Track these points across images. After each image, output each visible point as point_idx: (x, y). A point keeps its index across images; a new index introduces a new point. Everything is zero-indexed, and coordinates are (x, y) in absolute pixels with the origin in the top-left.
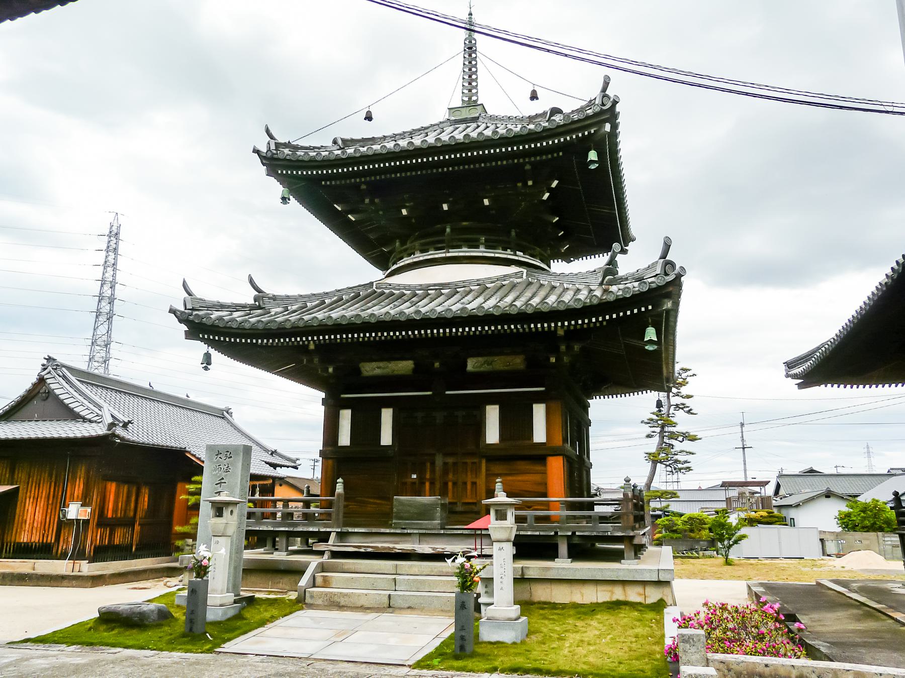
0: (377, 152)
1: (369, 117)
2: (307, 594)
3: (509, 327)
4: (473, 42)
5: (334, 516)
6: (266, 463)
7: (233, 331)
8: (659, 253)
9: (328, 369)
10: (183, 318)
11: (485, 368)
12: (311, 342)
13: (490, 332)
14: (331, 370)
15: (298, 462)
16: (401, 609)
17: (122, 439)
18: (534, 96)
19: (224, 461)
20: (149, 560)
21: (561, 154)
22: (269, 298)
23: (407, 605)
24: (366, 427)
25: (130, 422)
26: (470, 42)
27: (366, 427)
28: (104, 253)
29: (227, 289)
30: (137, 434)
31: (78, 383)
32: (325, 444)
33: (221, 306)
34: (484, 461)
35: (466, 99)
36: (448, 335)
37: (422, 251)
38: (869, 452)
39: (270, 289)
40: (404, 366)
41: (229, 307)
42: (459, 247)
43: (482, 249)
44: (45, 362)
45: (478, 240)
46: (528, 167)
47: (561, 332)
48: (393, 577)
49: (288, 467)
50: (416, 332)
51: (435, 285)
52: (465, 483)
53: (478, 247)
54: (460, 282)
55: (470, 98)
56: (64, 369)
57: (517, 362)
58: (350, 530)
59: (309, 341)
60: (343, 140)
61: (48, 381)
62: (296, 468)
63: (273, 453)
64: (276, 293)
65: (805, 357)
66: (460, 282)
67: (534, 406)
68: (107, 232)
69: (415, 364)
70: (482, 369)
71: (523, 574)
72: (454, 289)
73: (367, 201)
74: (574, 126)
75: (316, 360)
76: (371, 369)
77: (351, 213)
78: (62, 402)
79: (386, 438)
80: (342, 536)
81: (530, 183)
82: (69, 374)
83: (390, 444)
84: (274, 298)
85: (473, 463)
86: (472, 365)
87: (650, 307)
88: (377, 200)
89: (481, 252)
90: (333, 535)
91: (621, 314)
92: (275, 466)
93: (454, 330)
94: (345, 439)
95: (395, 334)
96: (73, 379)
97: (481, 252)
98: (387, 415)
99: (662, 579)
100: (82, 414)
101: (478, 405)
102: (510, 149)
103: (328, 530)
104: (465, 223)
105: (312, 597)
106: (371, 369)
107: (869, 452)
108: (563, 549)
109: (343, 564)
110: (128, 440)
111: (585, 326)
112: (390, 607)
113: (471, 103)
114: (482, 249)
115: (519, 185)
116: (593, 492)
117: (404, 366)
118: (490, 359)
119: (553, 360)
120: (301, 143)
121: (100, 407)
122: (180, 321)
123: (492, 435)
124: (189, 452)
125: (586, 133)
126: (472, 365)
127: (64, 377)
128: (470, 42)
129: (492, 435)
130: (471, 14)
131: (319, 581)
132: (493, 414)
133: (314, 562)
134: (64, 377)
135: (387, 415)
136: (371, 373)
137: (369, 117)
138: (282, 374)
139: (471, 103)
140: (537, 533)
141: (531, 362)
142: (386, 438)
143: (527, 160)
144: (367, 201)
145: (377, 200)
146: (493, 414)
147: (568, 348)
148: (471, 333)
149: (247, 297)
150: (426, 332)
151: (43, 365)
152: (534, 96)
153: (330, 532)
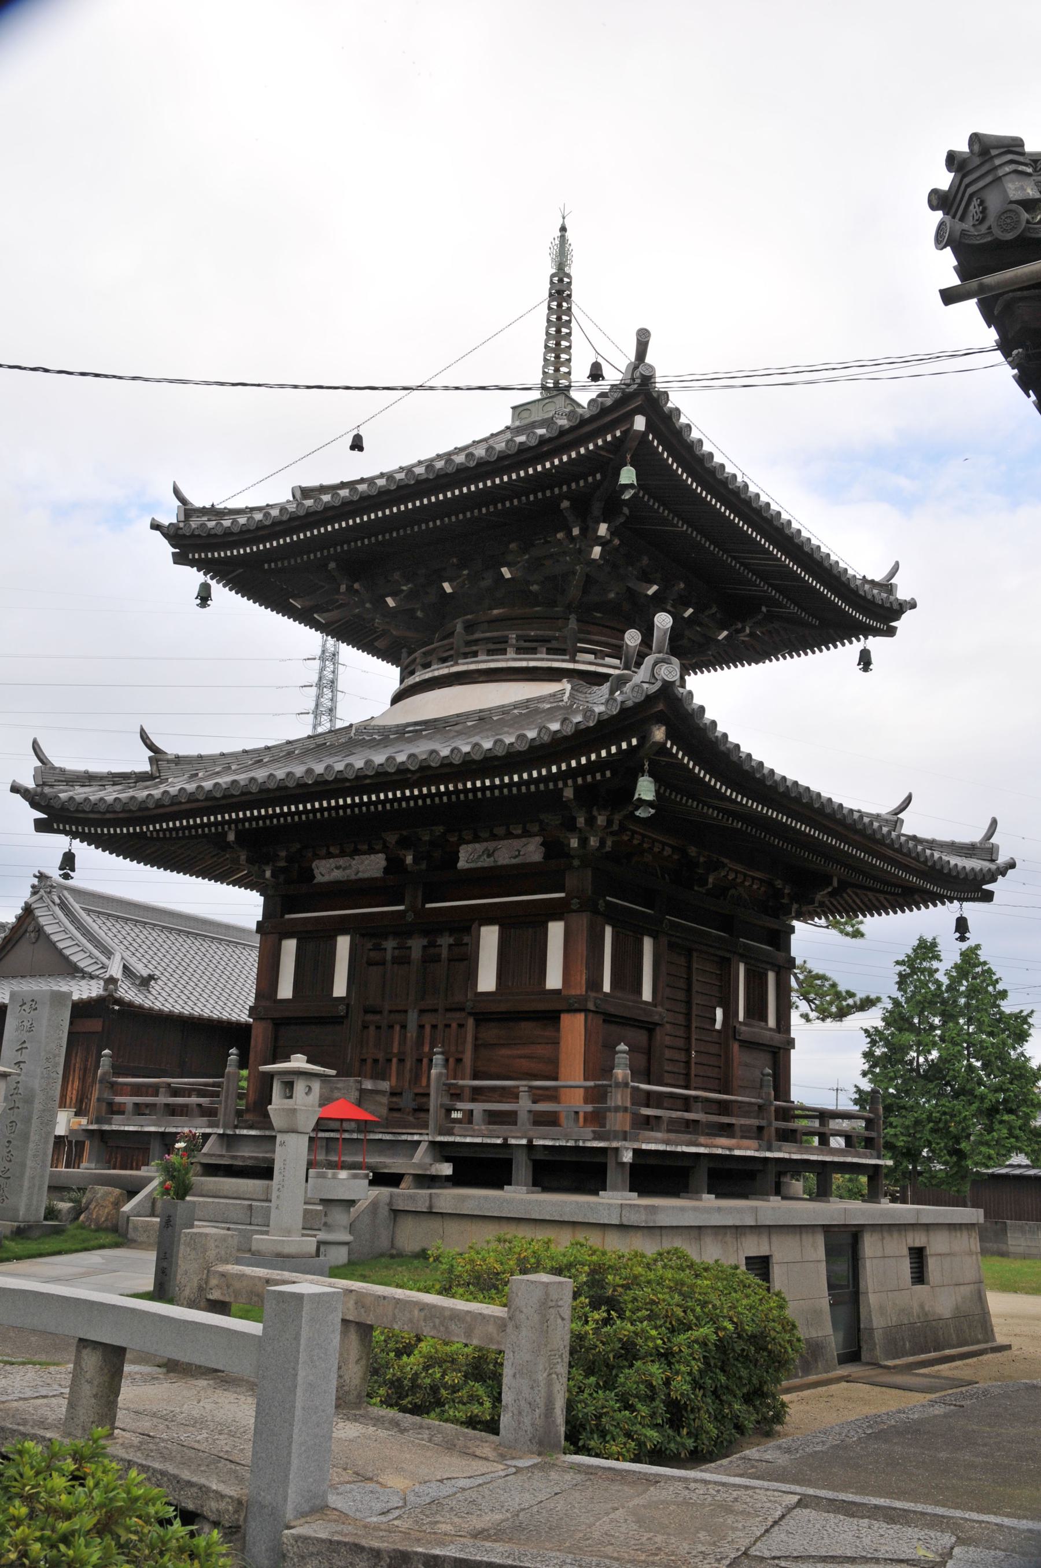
0: (312, 510)
1: (357, 444)
2: (131, 1225)
4: (566, 280)
10: (34, 799)
11: (487, 862)
18: (357, 444)
22: (169, 761)
24: (314, 969)
25: (151, 977)
26: (561, 281)
27: (314, 969)
28: (314, 691)
30: (163, 999)
31: (83, 914)
32: (258, 996)
34: (471, 1022)
39: (171, 747)
40: (371, 866)
43: (511, 653)
44: (36, 881)
45: (505, 640)
48: (249, 1203)
51: (416, 724)
53: (504, 652)
56: (66, 893)
61: (37, 913)
64: (182, 753)
68: (319, 653)
69: (387, 859)
70: (479, 864)
71: (431, 1207)
73: (343, 588)
78: (53, 944)
81: (576, 531)
82: (71, 900)
83: (344, 995)
84: (178, 760)
86: (468, 857)
89: (511, 661)
94: (286, 990)
96: (76, 906)
97: (511, 661)
100: (81, 965)
101: (465, 927)
104: (495, 612)
105: (135, 1229)
106: (327, 871)
108: (522, 1169)
114: (511, 653)
115: (560, 536)
117: (371, 866)
118: (491, 845)
120: (232, 505)
121: (108, 953)
126: (468, 857)
127: (63, 906)
128: (561, 281)
130: (563, 229)
134: (63, 906)
136: (326, 878)
138: (234, 883)
140: (478, 1140)
141: (554, 849)
144: (343, 588)
145: (356, 586)
149: (140, 762)
151: (33, 887)
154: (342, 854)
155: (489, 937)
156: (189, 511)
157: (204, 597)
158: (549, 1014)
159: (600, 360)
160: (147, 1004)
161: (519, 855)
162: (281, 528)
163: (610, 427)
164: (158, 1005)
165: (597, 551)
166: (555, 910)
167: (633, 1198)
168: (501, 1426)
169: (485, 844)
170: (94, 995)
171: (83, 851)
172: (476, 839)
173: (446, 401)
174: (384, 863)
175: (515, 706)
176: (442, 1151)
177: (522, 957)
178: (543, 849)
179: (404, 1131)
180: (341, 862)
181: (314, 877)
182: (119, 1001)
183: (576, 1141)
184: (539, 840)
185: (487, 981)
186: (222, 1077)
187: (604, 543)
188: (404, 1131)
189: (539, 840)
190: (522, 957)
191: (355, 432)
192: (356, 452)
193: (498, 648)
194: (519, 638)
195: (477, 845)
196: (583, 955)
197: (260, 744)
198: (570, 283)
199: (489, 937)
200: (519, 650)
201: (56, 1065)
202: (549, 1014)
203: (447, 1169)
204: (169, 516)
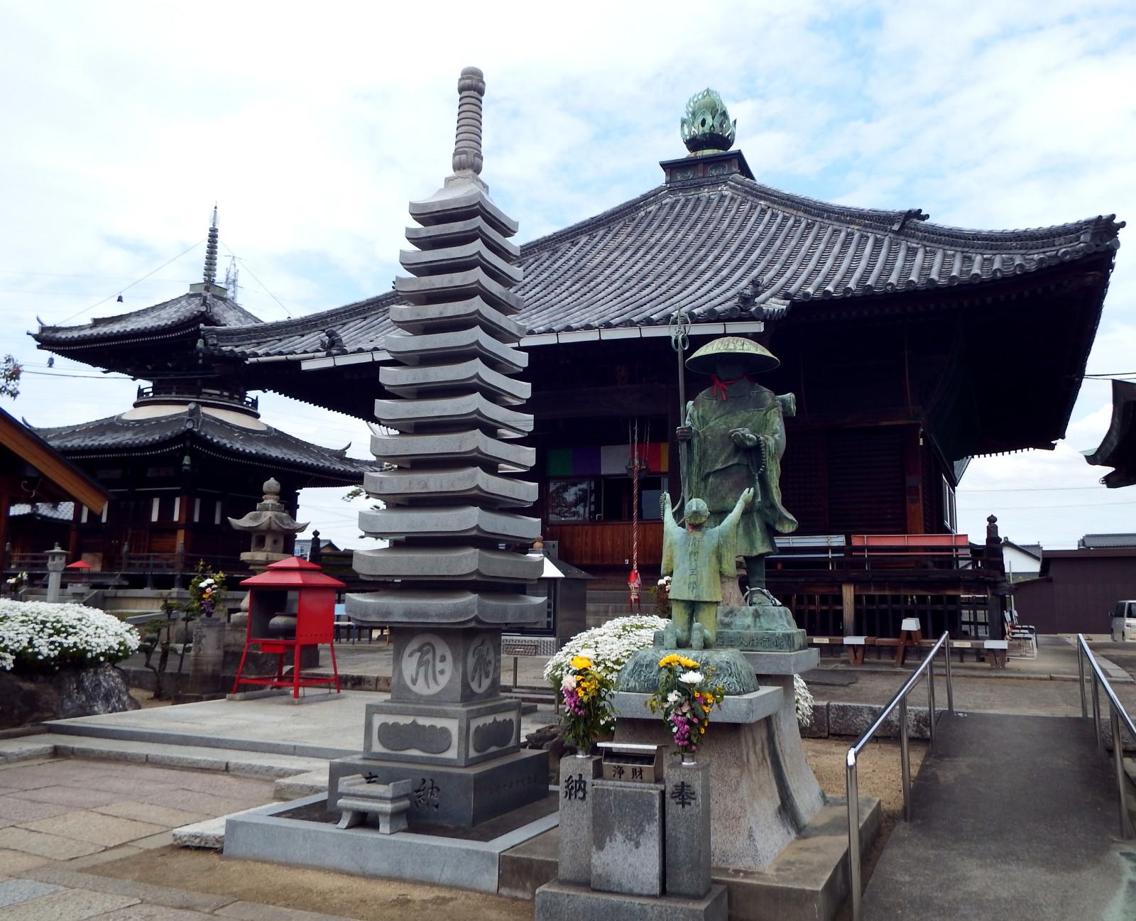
1: (120, 299)
18: (120, 299)
43: (174, 394)
108: (150, 581)
114: (174, 394)
155: (156, 504)
156: (44, 329)
157: (51, 363)
158: (174, 528)
160: (55, 516)
162: (30, 434)
163: (193, 326)
164: (61, 517)
165: (200, 361)
166: (176, 494)
168: (17, 602)
170: (26, 512)
171: (57, 357)
173: (153, 287)
175: (171, 416)
176: (124, 577)
177: (166, 511)
182: (40, 515)
185: (155, 518)
190: (166, 511)
192: (123, 299)
196: (187, 510)
197: (75, 424)
199: (156, 504)
201: (391, 414)
202: (174, 528)
203: (126, 583)
204: (36, 331)
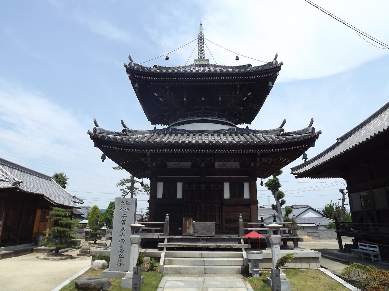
1: (167, 59)
3: (142, 151)
5: (164, 231)
6: (73, 201)
7: (127, 145)
8: (309, 124)
9: (153, 164)
11: (224, 167)
12: (148, 152)
13: (223, 152)
14: (154, 164)
15: (83, 201)
16: (210, 274)
17: (20, 190)
18: (237, 59)
19: (125, 207)
20: (23, 245)
21: (254, 82)
22: (130, 131)
23: (213, 272)
24: (170, 190)
29: (112, 126)
33: (111, 133)
35: (199, 57)
36: (205, 152)
37: (191, 117)
38: (269, 200)
39: (131, 127)
40: (187, 164)
41: (114, 133)
42: (208, 116)
46: (238, 86)
47: (148, 154)
49: (79, 203)
50: (230, 150)
51: (201, 131)
52: (215, 216)
53: (215, 117)
54: (205, 132)
55: (201, 57)
57: (236, 165)
58: (174, 237)
59: (148, 151)
60: (159, 66)
62: (82, 204)
63: (74, 197)
65: (298, 167)
66: (205, 132)
67: (244, 183)
69: (192, 164)
70: (221, 167)
72: (206, 132)
74: (270, 71)
75: (149, 160)
76: (171, 165)
77: (162, 98)
79: (179, 195)
80: (169, 240)
81: (238, 93)
85: (218, 207)
87: (306, 145)
88: (172, 93)
89: (224, 120)
90: (166, 240)
91: (295, 147)
92: (76, 202)
93: (205, 150)
94: (160, 195)
95: (223, 151)
98: (180, 186)
99: (316, 257)
102: (248, 78)
103: (163, 237)
104: (207, 107)
105: (167, 270)
106: (171, 165)
107: (269, 200)
109: (175, 253)
110: (22, 190)
111: (168, 152)
112: (205, 273)
113: (201, 58)
115: (233, 93)
116: (260, 218)
117: (187, 164)
119: (253, 165)
122: (91, 138)
123: (227, 195)
124: (45, 196)
125: (269, 75)
126: (217, 165)
129: (227, 195)
131: (167, 262)
132: (227, 187)
133: (163, 253)
135: (180, 186)
137: (167, 59)
139: (201, 58)
142: (179, 195)
143: (238, 83)
144: (168, 93)
146: (227, 187)
147: (260, 160)
148: (165, 152)
150: (201, 151)
152: (237, 59)
153: (164, 239)
154: (177, 161)
159: (238, 55)
161: (233, 166)
167: (48, 222)
169: (223, 163)
172: (220, 161)
174: (191, 165)
178: (240, 165)
179: (221, 235)
180: (176, 163)
181: (167, 166)
183: (285, 237)
184: (238, 163)
186: (164, 222)
187: (248, 97)
188: (221, 235)
189: (238, 163)
191: (166, 55)
192: (237, 61)
193: (214, 116)
194: (218, 114)
195: (220, 163)
198: (203, 35)
200: (218, 117)
